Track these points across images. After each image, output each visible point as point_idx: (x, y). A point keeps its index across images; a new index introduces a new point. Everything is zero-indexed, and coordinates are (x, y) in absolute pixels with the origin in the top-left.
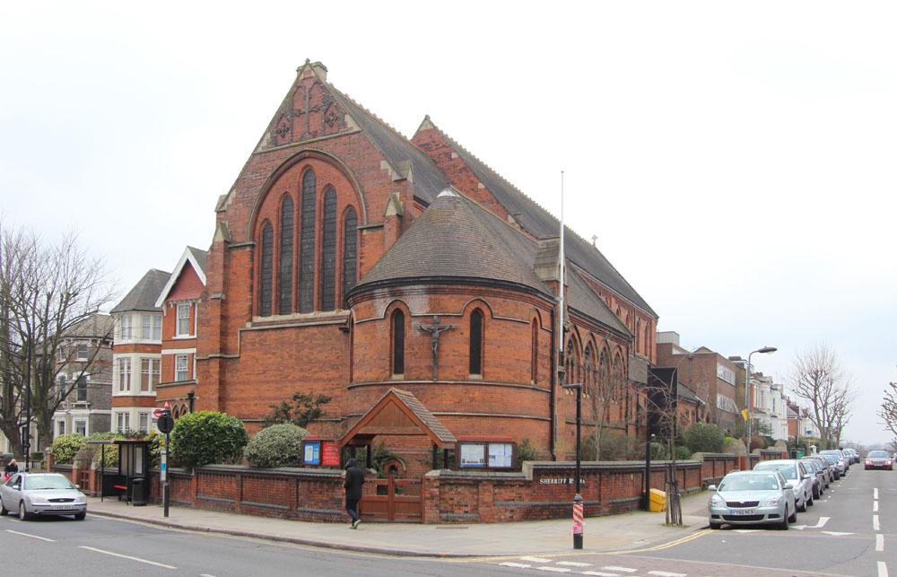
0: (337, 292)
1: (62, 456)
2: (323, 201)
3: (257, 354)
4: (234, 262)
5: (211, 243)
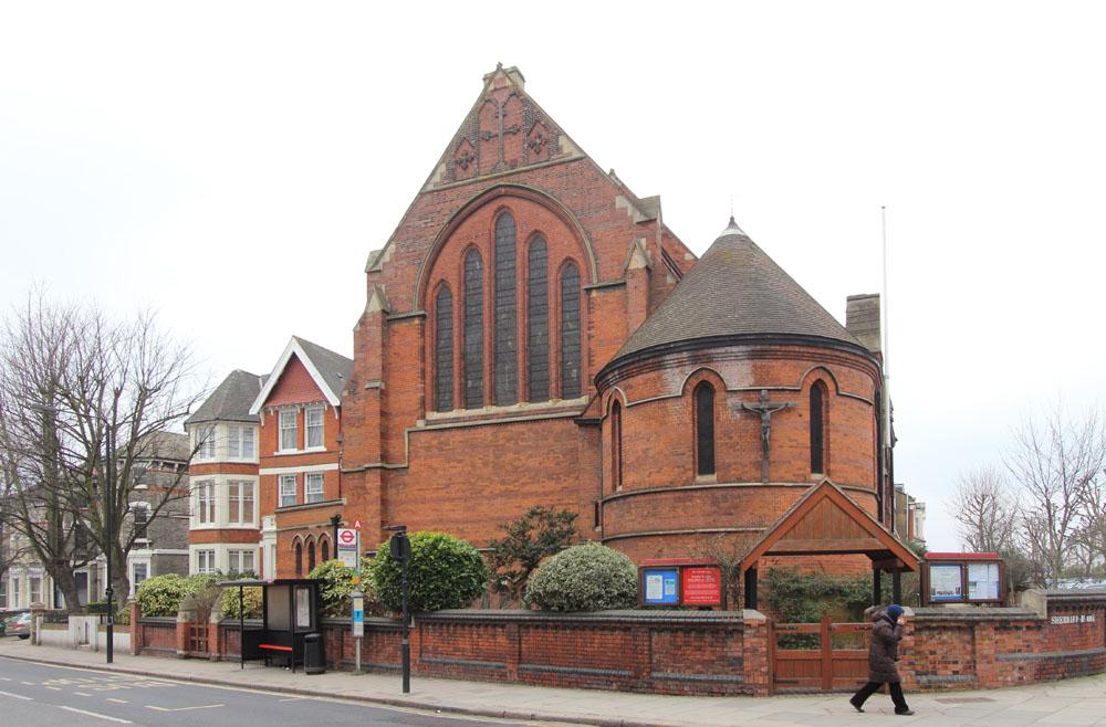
0: (553, 376)
1: (154, 606)
3: (435, 463)
4: (396, 339)
5: (363, 311)
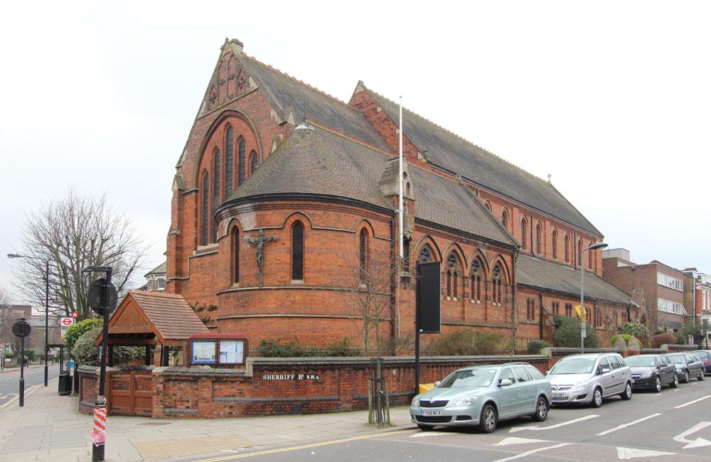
2: (238, 150)
